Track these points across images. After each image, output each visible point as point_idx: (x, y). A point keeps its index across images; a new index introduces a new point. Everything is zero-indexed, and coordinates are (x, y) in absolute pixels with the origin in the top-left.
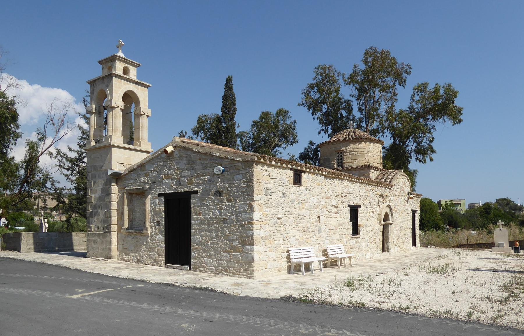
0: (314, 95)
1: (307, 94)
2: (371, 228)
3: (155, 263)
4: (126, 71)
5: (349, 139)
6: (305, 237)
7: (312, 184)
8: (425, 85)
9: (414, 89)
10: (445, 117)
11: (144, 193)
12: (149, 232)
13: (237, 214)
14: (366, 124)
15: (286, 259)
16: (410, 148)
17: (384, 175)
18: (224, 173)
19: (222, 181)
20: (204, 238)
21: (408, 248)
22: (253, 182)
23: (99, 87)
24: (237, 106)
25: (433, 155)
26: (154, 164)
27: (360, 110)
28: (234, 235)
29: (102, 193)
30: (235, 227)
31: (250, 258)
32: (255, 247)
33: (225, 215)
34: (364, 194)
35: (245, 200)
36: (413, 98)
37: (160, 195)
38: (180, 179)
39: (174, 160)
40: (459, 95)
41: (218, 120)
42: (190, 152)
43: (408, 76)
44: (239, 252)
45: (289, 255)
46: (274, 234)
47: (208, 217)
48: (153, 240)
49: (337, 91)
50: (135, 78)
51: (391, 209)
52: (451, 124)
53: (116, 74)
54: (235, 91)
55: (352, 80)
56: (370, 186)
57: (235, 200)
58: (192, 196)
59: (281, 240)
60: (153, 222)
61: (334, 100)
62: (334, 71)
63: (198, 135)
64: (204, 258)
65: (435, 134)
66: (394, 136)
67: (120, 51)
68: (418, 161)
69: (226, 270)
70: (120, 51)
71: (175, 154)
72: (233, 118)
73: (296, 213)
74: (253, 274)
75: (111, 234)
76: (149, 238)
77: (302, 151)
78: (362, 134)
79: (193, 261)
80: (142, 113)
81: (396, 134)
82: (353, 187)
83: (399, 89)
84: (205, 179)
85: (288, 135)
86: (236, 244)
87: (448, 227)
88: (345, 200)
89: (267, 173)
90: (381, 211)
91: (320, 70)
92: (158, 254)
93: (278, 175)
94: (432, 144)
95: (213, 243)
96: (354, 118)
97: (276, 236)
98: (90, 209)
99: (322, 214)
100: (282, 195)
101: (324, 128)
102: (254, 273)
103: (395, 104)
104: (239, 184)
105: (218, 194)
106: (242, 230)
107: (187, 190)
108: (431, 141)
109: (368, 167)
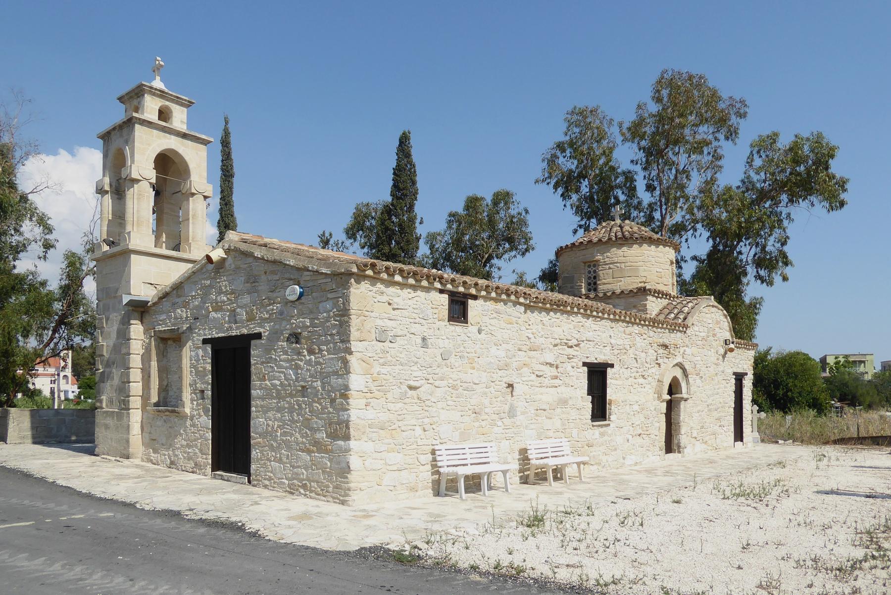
0: (567, 164)
1: (552, 161)
2: (636, 407)
3: (197, 468)
4: (164, 114)
5: (610, 239)
6: (477, 424)
7: (493, 322)
8: (773, 138)
9: (751, 146)
10: (813, 198)
11: (180, 338)
12: (187, 410)
13: (324, 377)
14: (662, 215)
15: (429, 467)
16: (744, 257)
17: (675, 307)
18: (303, 299)
19: (301, 314)
20: (270, 423)
21: (725, 444)
22: (349, 315)
23: (116, 142)
24: (419, 185)
25: (788, 270)
26: (195, 283)
27: (650, 188)
28: (318, 418)
29: (118, 338)
30: (320, 404)
31: (344, 465)
32: (352, 444)
33: (304, 380)
34: (620, 342)
35: (336, 351)
36: (750, 162)
37: (205, 341)
38: (234, 311)
39: (227, 276)
40: (838, 154)
41: (388, 211)
42: (250, 260)
44: (326, 451)
45: (434, 460)
46: (400, 418)
47: (278, 383)
48: (193, 425)
49: (608, 153)
50: (183, 128)
51: (684, 371)
52: (825, 211)
53: (140, 119)
54: (415, 158)
55: (635, 132)
56: (635, 327)
57: (321, 350)
58: (253, 342)
59: (418, 430)
60: (194, 392)
61: (601, 169)
62: (600, 116)
63: (355, 240)
64: (271, 461)
65: (791, 229)
66: (713, 236)
67: (158, 78)
68: (759, 282)
69: (304, 487)
70: (158, 78)
71: (227, 264)
72: (411, 208)
73: (454, 376)
74: (347, 495)
75: (129, 414)
76: (189, 422)
77: (545, 265)
78: (635, 229)
79: (253, 467)
80: (193, 191)
81: (718, 232)
82: (594, 327)
83: (726, 147)
84: (273, 310)
85: (514, 238)
86: (322, 435)
87: (838, 404)
88: (575, 353)
89: (385, 298)
90: (663, 375)
91: (575, 117)
92: (201, 451)
93: (410, 302)
94: (785, 248)
95: (284, 434)
96: (640, 203)
97: (405, 423)
98: (100, 367)
99: (517, 380)
100: (419, 341)
101: (583, 223)
102: (350, 493)
103: (718, 175)
104: (327, 320)
105: (293, 340)
106: (331, 410)
107: (245, 331)
108: (784, 244)
109: (643, 292)
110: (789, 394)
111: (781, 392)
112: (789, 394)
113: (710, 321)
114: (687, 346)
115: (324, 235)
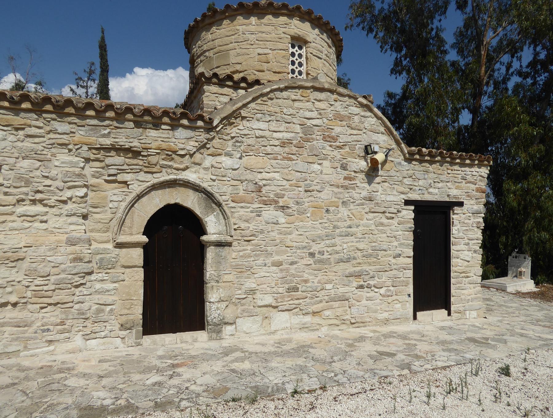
113: (314, 114)
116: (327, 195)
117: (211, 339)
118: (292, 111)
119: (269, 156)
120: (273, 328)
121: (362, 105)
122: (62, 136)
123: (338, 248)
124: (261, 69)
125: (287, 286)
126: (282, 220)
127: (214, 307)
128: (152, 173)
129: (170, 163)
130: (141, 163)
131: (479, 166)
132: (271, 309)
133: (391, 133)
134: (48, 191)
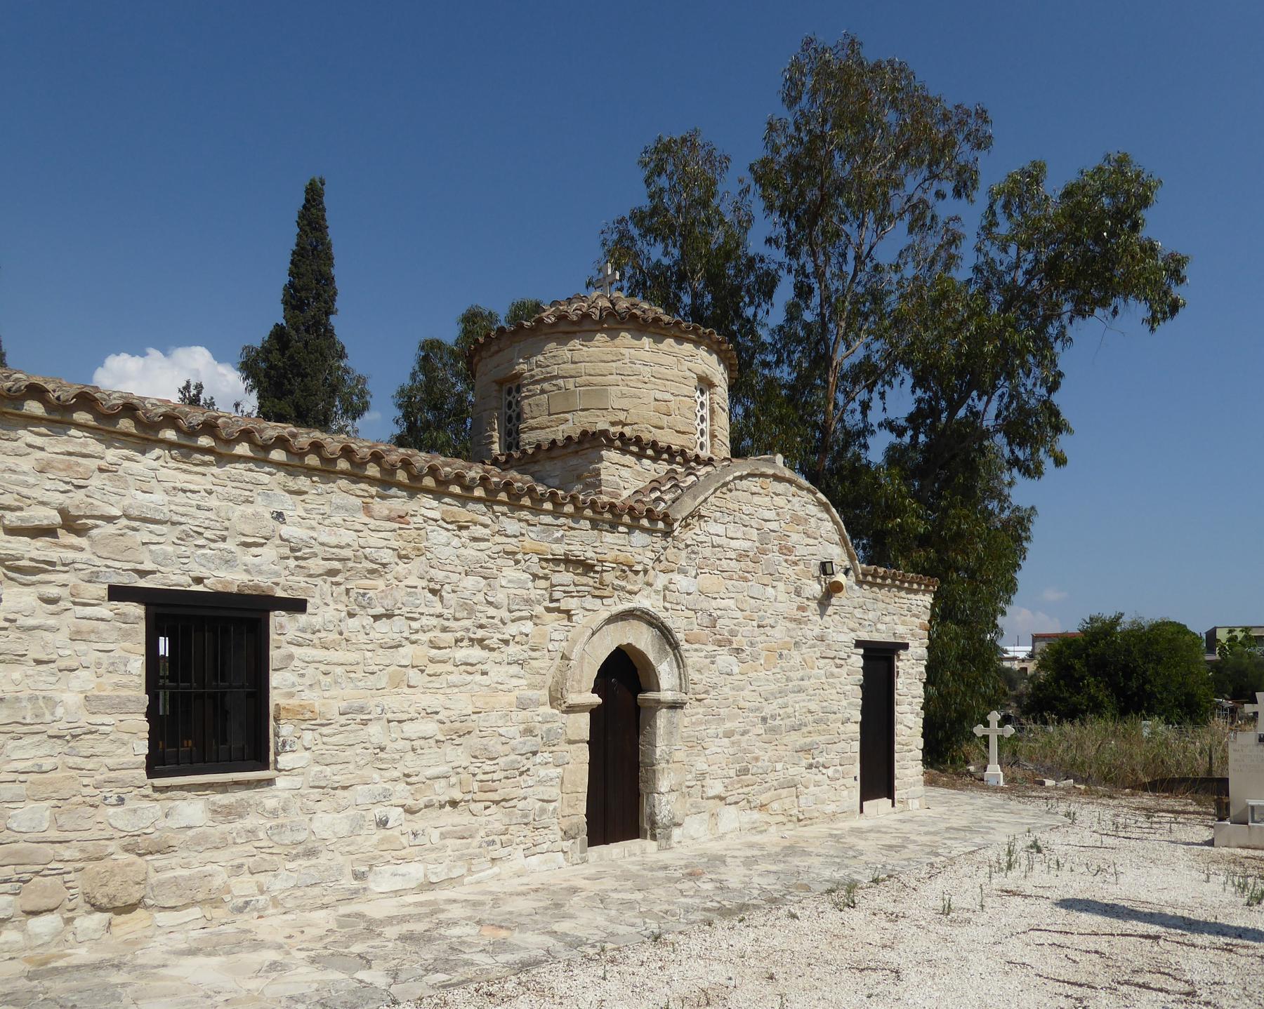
8: (1034, 175)
40: (1158, 196)
43: (982, 154)
65: (1066, 359)
66: (919, 381)
94: (1056, 398)
108: (1053, 388)
110: (1148, 687)
111: (1134, 684)
112: (1148, 687)
113: (771, 515)
114: (682, 571)
115: (187, 388)
116: (780, 633)
117: (660, 849)
118: (750, 510)
119: (724, 574)
120: (722, 829)
121: (820, 503)
122: (509, 540)
123: (790, 710)
124: (660, 424)
125: (737, 766)
126: (736, 670)
127: (664, 799)
128: (602, 598)
129: (623, 583)
130: (591, 582)
131: (925, 592)
132: (717, 801)
133: (846, 545)
134: (492, 625)
